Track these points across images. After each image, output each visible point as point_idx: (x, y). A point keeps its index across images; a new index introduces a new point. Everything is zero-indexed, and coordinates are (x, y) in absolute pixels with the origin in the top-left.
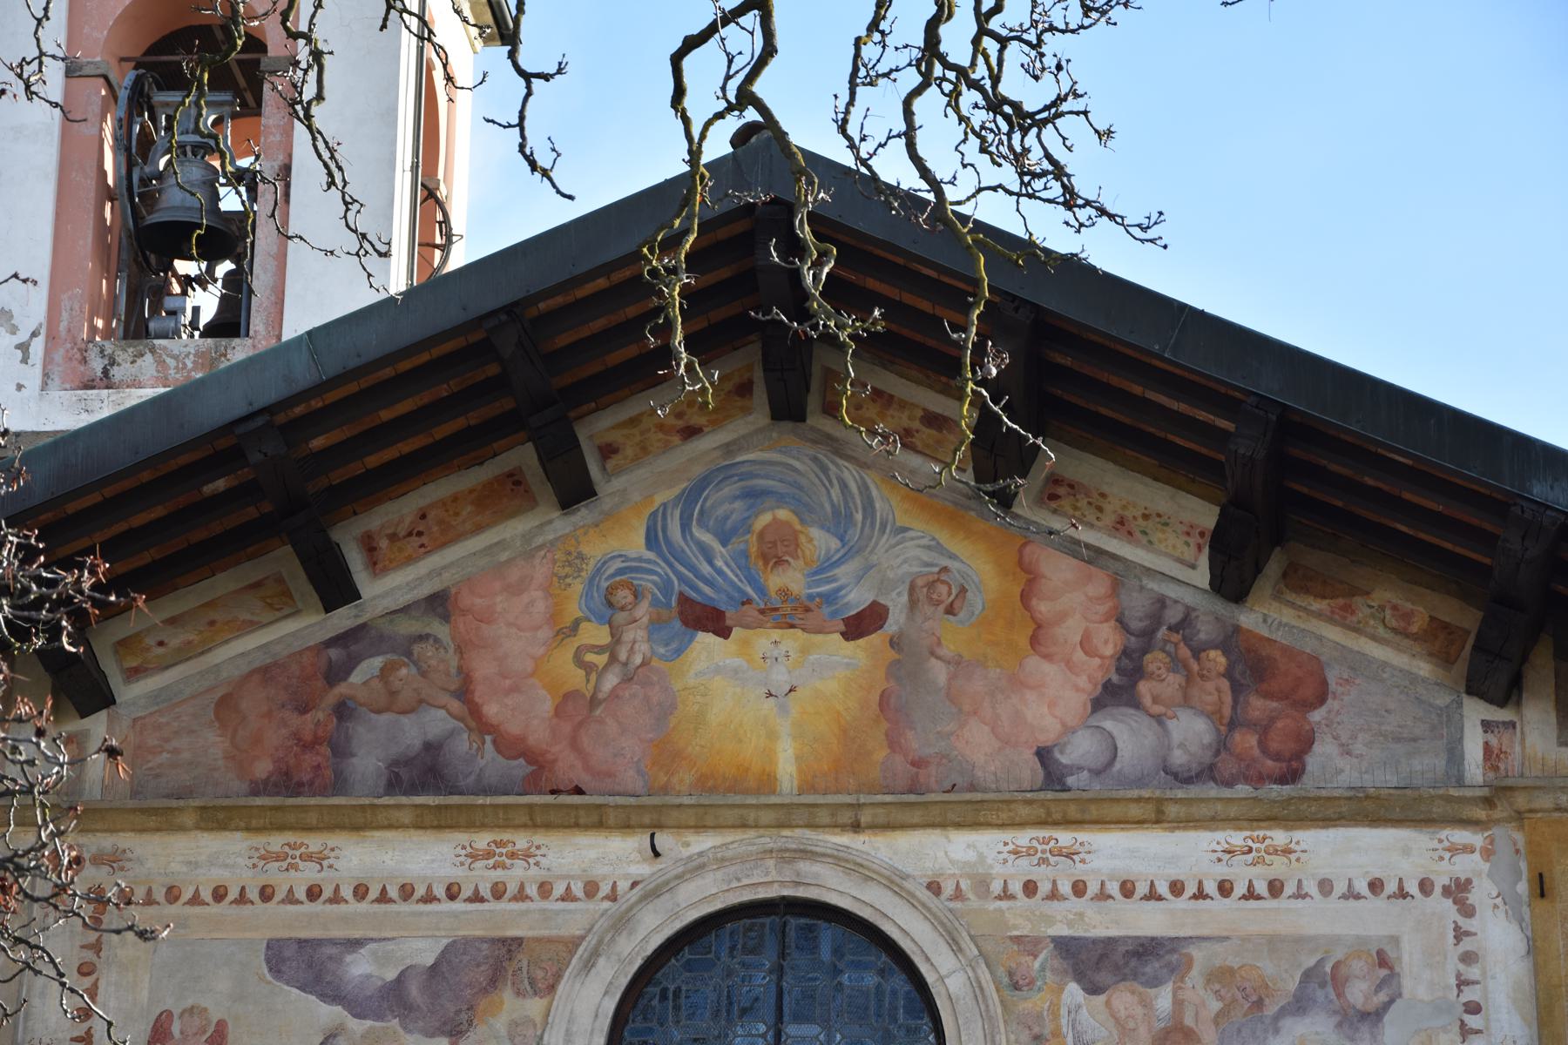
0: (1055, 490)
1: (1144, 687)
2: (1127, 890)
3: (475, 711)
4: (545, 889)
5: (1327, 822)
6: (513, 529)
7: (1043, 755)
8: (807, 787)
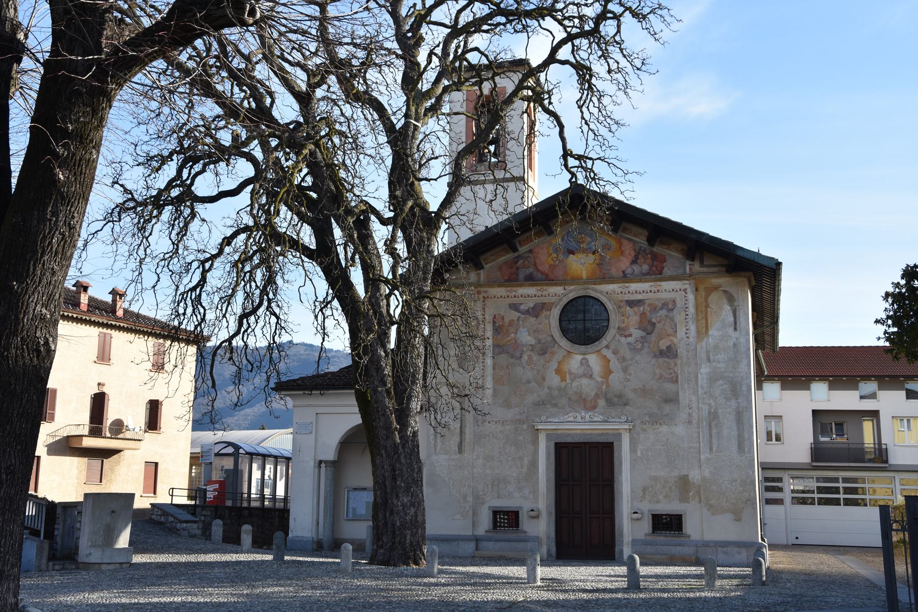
0: (624, 230)
1: (639, 261)
2: (636, 292)
3: (537, 268)
4: (549, 295)
5: (666, 281)
6: (542, 239)
7: (623, 272)
8: (588, 279)
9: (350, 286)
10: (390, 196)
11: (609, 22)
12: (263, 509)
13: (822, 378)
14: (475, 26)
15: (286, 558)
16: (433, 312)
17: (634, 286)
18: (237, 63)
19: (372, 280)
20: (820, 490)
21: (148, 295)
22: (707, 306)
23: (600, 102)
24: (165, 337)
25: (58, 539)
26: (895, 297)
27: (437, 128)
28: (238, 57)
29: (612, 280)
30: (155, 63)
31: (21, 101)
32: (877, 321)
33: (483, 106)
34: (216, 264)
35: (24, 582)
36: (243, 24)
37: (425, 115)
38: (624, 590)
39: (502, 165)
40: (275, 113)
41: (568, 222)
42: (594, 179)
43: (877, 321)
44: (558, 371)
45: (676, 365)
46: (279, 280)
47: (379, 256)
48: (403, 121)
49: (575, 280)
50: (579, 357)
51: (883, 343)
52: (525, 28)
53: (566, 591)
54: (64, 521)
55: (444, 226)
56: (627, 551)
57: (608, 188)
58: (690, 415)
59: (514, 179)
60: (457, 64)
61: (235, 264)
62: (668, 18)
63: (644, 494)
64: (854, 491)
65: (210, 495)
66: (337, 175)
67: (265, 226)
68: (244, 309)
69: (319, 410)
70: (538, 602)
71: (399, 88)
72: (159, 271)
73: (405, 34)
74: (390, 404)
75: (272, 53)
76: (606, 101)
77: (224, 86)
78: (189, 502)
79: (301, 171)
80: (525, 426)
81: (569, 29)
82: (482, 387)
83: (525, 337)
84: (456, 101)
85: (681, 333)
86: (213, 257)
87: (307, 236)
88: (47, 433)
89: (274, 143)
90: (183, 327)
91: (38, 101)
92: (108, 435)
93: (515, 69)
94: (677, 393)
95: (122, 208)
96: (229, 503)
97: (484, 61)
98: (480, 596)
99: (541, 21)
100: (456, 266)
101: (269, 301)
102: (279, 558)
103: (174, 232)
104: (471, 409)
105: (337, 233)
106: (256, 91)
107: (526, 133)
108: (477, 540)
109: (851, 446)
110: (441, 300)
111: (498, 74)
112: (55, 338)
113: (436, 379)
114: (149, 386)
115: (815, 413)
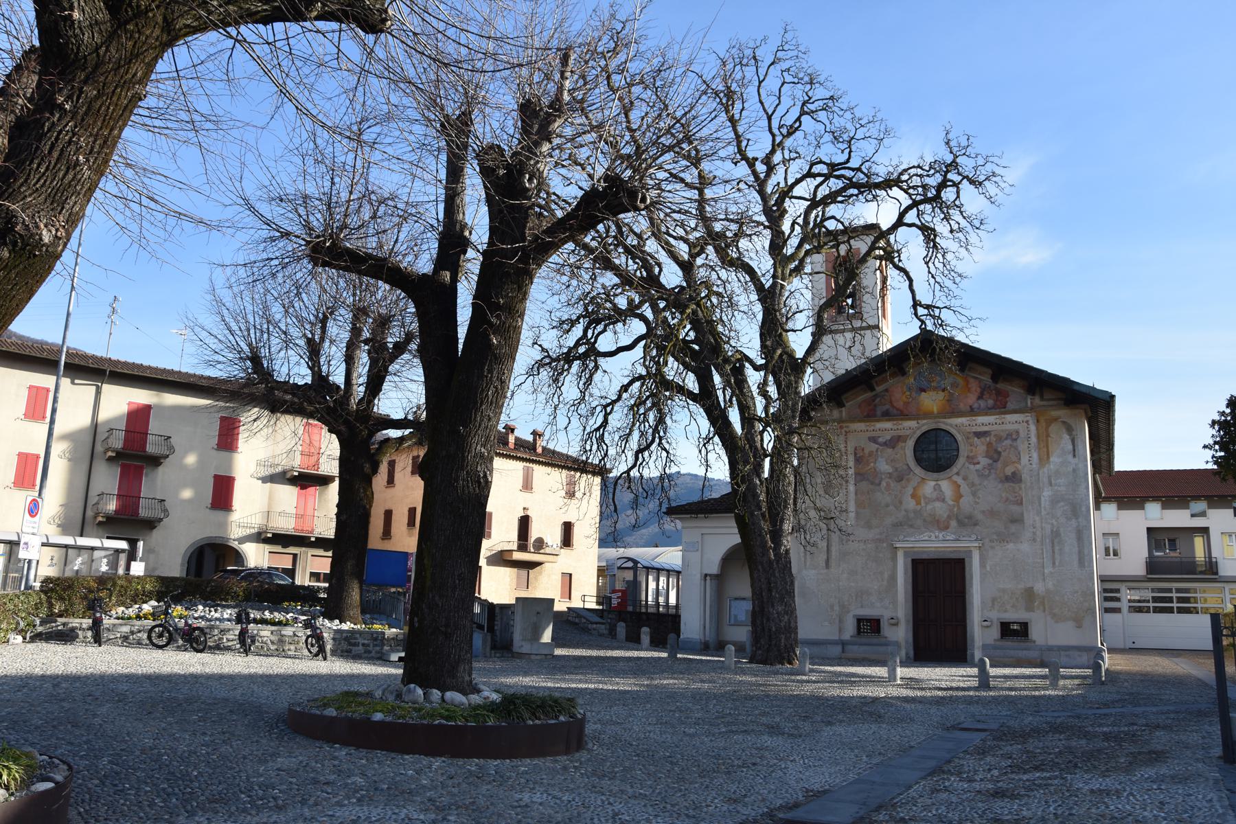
6: (896, 379)
9: (728, 424)
10: (762, 346)
11: (949, 189)
12: (658, 614)
13: (1155, 499)
14: (832, 198)
15: (679, 656)
16: (801, 445)
17: (980, 419)
18: (632, 241)
19: (748, 418)
20: (1155, 600)
21: (562, 435)
22: (1048, 436)
23: (944, 258)
24: (576, 470)
25: (498, 633)
26: (1221, 425)
27: (801, 285)
28: (632, 235)
29: (961, 414)
30: (566, 246)
31: (465, 283)
32: (1205, 447)
33: (840, 265)
34: (616, 408)
35: (475, 665)
36: (636, 209)
37: (790, 275)
38: (975, 689)
39: (859, 315)
40: (663, 280)
41: (919, 364)
42: (941, 325)
43: (1205, 447)
44: (914, 496)
45: (1020, 489)
46: (668, 421)
47: (753, 398)
48: (771, 281)
49: (928, 415)
50: (933, 483)
51: (1211, 466)
52: (875, 197)
53: (923, 689)
54: (502, 619)
55: (809, 370)
56: (978, 655)
57: (954, 333)
58: (1034, 533)
59: (870, 327)
60: (817, 231)
61: (631, 408)
62: (1003, 185)
63: (993, 604)
64: (1187, 600)
65: (615, 602)
66: (715, 329)
67: (655, 375)
68: (639, 446)
69: (704, 531)
70: (898, 698)
71: (767, 254)
72: (569, 415)
73: (771, 208)
74: (765, 526)
75: (659, 230)
76: (949, 256)
77: (620, 260)
78: (597, 607)
79: (685, 327)
80: (885, 545)
81: (914, 197)
82: (846, 511)
83: (883, 466)
84: (816, 262)
85: (1025, 460)
86: (614, 402)
87: (691, 383)
88: (487, 547)
89: (662, 304)
90: (590, 461)
91: (478, 283)
92: (532, 550)
93: (867, 232)
94: (1022, 514)
95: (540, 364)
96: (630, 609)
97: (840, 227)
98: (847, 692)
99: (889, 191)
100: (821, 404)
101: (660, 438)
102: (672, 655)
103: (581, 383)
104: (836, 530)
105: (717, 379)
106: (647, 263)
107: (879, 288)
108: (843, 644)
109: (1183, 560)
110: (808, 435)
111: (853, 238)
112: (491, 471)
113: (805, 504)
114: (563, 511)
115: (1149, 530)
